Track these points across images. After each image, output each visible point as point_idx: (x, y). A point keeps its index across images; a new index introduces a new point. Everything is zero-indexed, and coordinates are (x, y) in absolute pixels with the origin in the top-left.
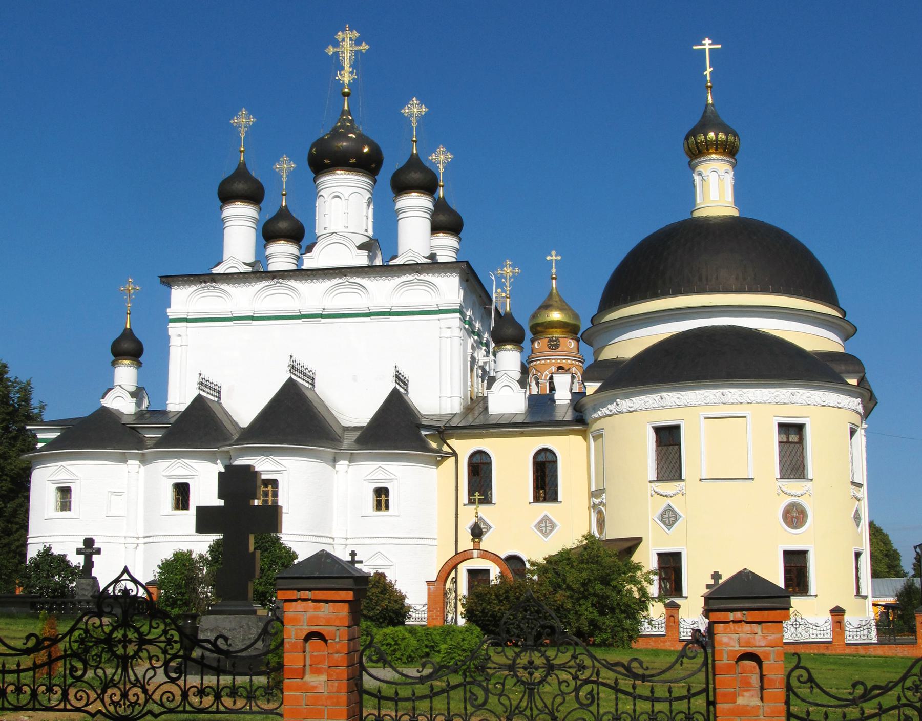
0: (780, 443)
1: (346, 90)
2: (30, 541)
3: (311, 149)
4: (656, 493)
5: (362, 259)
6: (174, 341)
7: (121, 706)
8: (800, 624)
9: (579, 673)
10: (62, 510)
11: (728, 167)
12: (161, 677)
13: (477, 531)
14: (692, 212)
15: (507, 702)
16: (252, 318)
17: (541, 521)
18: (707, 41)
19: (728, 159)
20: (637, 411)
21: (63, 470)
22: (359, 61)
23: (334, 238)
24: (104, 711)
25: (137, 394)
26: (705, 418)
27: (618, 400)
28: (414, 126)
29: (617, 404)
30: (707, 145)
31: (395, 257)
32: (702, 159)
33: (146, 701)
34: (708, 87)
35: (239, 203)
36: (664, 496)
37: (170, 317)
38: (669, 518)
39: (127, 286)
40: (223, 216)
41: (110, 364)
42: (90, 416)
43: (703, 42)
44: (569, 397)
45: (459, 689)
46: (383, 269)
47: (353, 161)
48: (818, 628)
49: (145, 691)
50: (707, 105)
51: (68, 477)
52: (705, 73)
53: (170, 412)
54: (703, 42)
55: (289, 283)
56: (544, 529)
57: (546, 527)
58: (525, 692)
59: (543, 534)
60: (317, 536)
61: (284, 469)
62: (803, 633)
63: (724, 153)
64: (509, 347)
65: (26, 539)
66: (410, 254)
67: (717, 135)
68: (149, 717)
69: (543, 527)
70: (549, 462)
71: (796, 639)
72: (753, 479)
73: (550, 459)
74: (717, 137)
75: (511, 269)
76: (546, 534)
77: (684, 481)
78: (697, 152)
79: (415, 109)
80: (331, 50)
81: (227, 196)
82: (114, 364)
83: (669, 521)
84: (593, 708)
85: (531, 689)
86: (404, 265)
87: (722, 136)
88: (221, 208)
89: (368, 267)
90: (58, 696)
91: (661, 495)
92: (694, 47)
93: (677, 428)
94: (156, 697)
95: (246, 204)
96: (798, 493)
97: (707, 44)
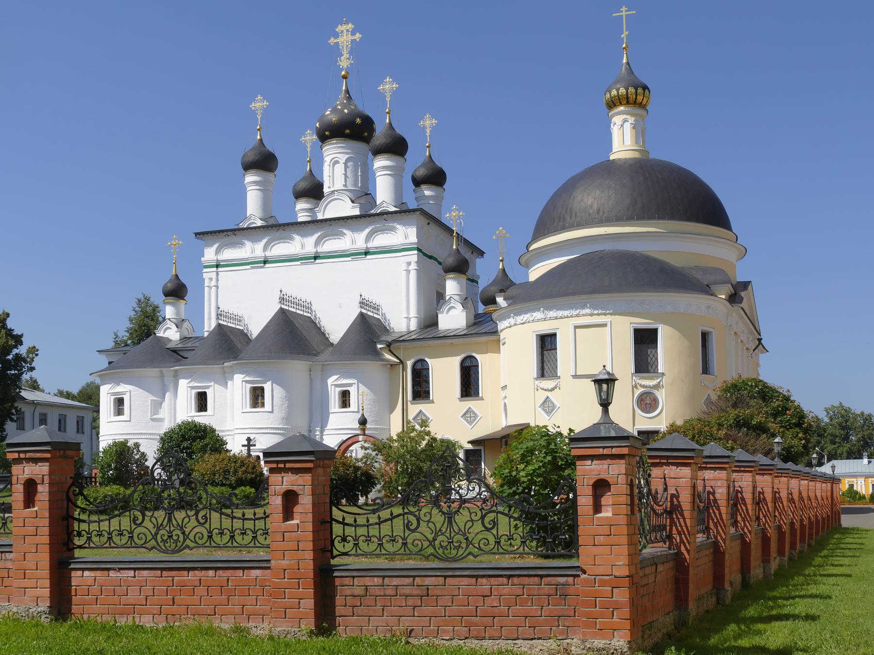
0: (556, 349)
7: (447, 549)
9: (483, 506)
10: (199, 412)
12: (478, 527)
15: (155, 522)
24: (436, 554)
28: (388, 100)
33: (185, 540)
45: (261, 521)
46: (363, 220)
47: (348, 131)
49: (183, 533)
58: (166, 515)
68: (471, 557)
80: (332, 41)
84: (494, 531)
85: (450, 517)
90: (351, 544)
92: (614, 15)
94: (191, 536)
97: (624, 12)
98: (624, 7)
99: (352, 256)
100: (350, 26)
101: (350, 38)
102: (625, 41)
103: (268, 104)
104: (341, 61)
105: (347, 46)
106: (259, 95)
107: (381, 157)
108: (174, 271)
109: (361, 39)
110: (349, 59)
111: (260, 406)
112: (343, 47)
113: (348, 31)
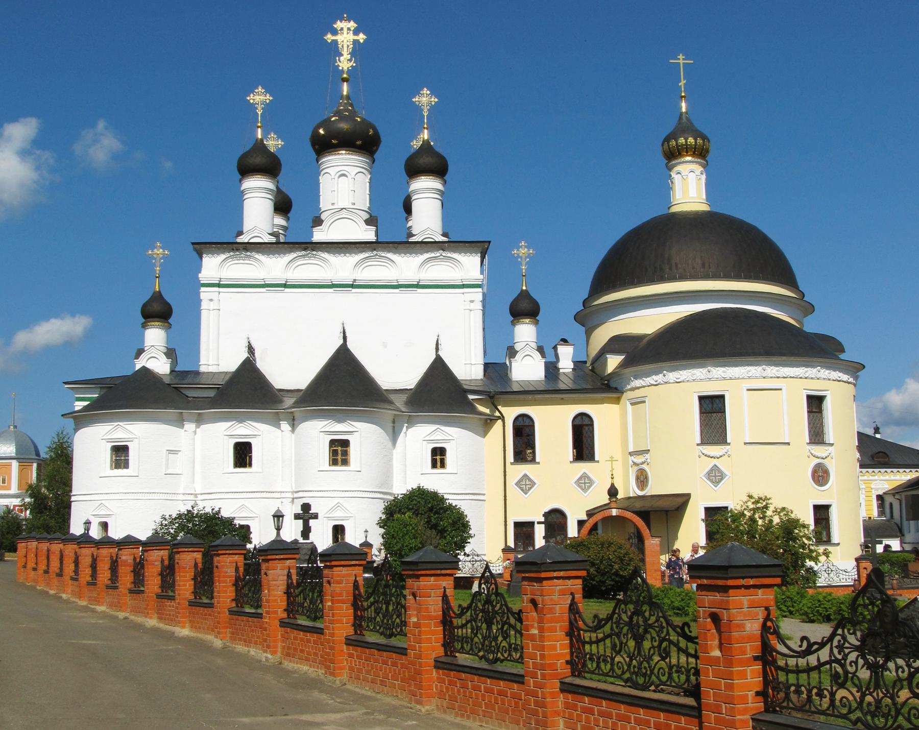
1: (345, 76)
2: (73, 499)
3: (318, 127)
4: (703, 454)
5: (369, 234)
6: (204, 305)
8: (832, 571)
10: (116, 468)
11: (698, 169)
13: (613, 491)
14: (669, 208)
16: (418, 286)
17: (580, 478)
18: (681, 57)
19: (699, 160)
20: (684, 382)
21: (119, 429)
22: (357, 50)
23: (344, 214)
25: (170, 353)
26: (748, 390)
27: (665, 372)
28: (426, 114)
29: (664, 376)
30: (678, 149)
31: (240, 233)
32: (679, 161)
34: (682, 97)
35: (423, 177)
36: (712, 457)
37: (201, 282)
38: (715, 476)
39: (155, 251)
40: (242, 189)
41: (141, 326)
42: (132, 374)
43: (679, 57)
44: (572, 365)
47: (359, 143)
48: (847, 574)
50: (681, 114)
51: (131, 436)
52: (680, 84)
53: (204, 373)
54: (679, 57)
55: (323, 255)
56: (583, 485)
57: (585, 483)
59: (583, 489)
60: (252, 492)
61: (356, 430)
62: (835, 578)
63: (694, 155)
64: (527, 320)
65: (70, 497)
66: (428, 232)
67: (686, 140)
69: (582, 483)
70: (588, 425)
71: (829, 583)
72: (788, 444)
73: (527, 424)
74: (686, 141)
75: (526, 250)
76: (585, 490)
77: (729, 444)
78: (672, 155)
79: (259, 98)
80: (329, 37)
81: (246, 169)
82: (144, 326)
83: (716, 479)
86: (422, 242)
87: (691, 140)
88: (240, 181)
89: (377, 242)
91: (709, 457)
93: (722, 397)
95: (262, 177)
96: (824, 455)
97: (681, 59)
98: (681, 55)
99: (401, 288)
100: (352, 25)
101: (351, 37)
102: (683, 90)
103: (271, 98)
104: (340, 62)
105: (348, 46)
106: (260, 87)
107: (426, 177)
108: (157, 287)
109: (365, 41)
110: (350, 60)
111: (340, 463)
112: (343, 46)
113: (349, 29)
